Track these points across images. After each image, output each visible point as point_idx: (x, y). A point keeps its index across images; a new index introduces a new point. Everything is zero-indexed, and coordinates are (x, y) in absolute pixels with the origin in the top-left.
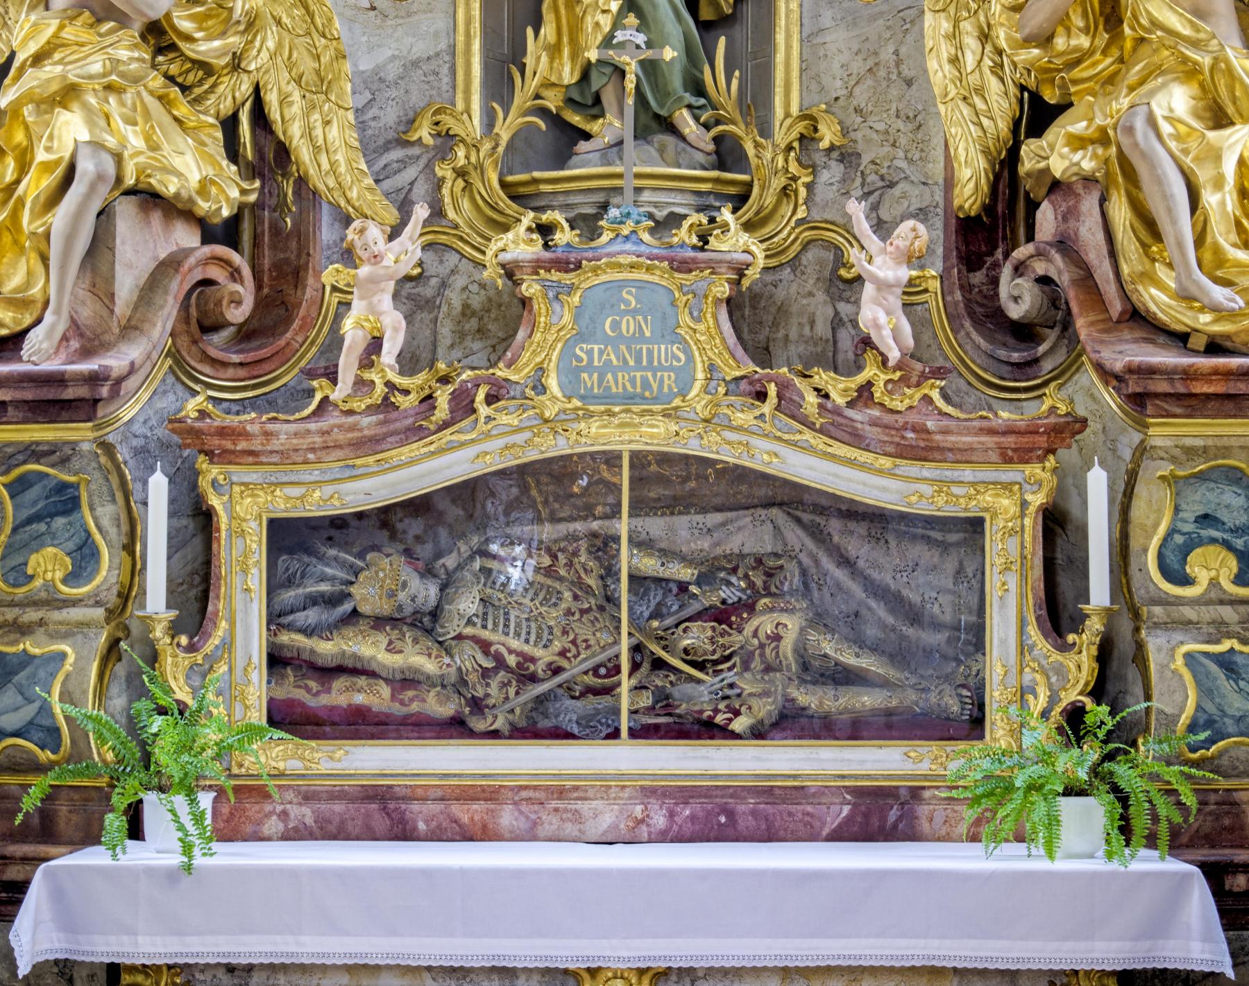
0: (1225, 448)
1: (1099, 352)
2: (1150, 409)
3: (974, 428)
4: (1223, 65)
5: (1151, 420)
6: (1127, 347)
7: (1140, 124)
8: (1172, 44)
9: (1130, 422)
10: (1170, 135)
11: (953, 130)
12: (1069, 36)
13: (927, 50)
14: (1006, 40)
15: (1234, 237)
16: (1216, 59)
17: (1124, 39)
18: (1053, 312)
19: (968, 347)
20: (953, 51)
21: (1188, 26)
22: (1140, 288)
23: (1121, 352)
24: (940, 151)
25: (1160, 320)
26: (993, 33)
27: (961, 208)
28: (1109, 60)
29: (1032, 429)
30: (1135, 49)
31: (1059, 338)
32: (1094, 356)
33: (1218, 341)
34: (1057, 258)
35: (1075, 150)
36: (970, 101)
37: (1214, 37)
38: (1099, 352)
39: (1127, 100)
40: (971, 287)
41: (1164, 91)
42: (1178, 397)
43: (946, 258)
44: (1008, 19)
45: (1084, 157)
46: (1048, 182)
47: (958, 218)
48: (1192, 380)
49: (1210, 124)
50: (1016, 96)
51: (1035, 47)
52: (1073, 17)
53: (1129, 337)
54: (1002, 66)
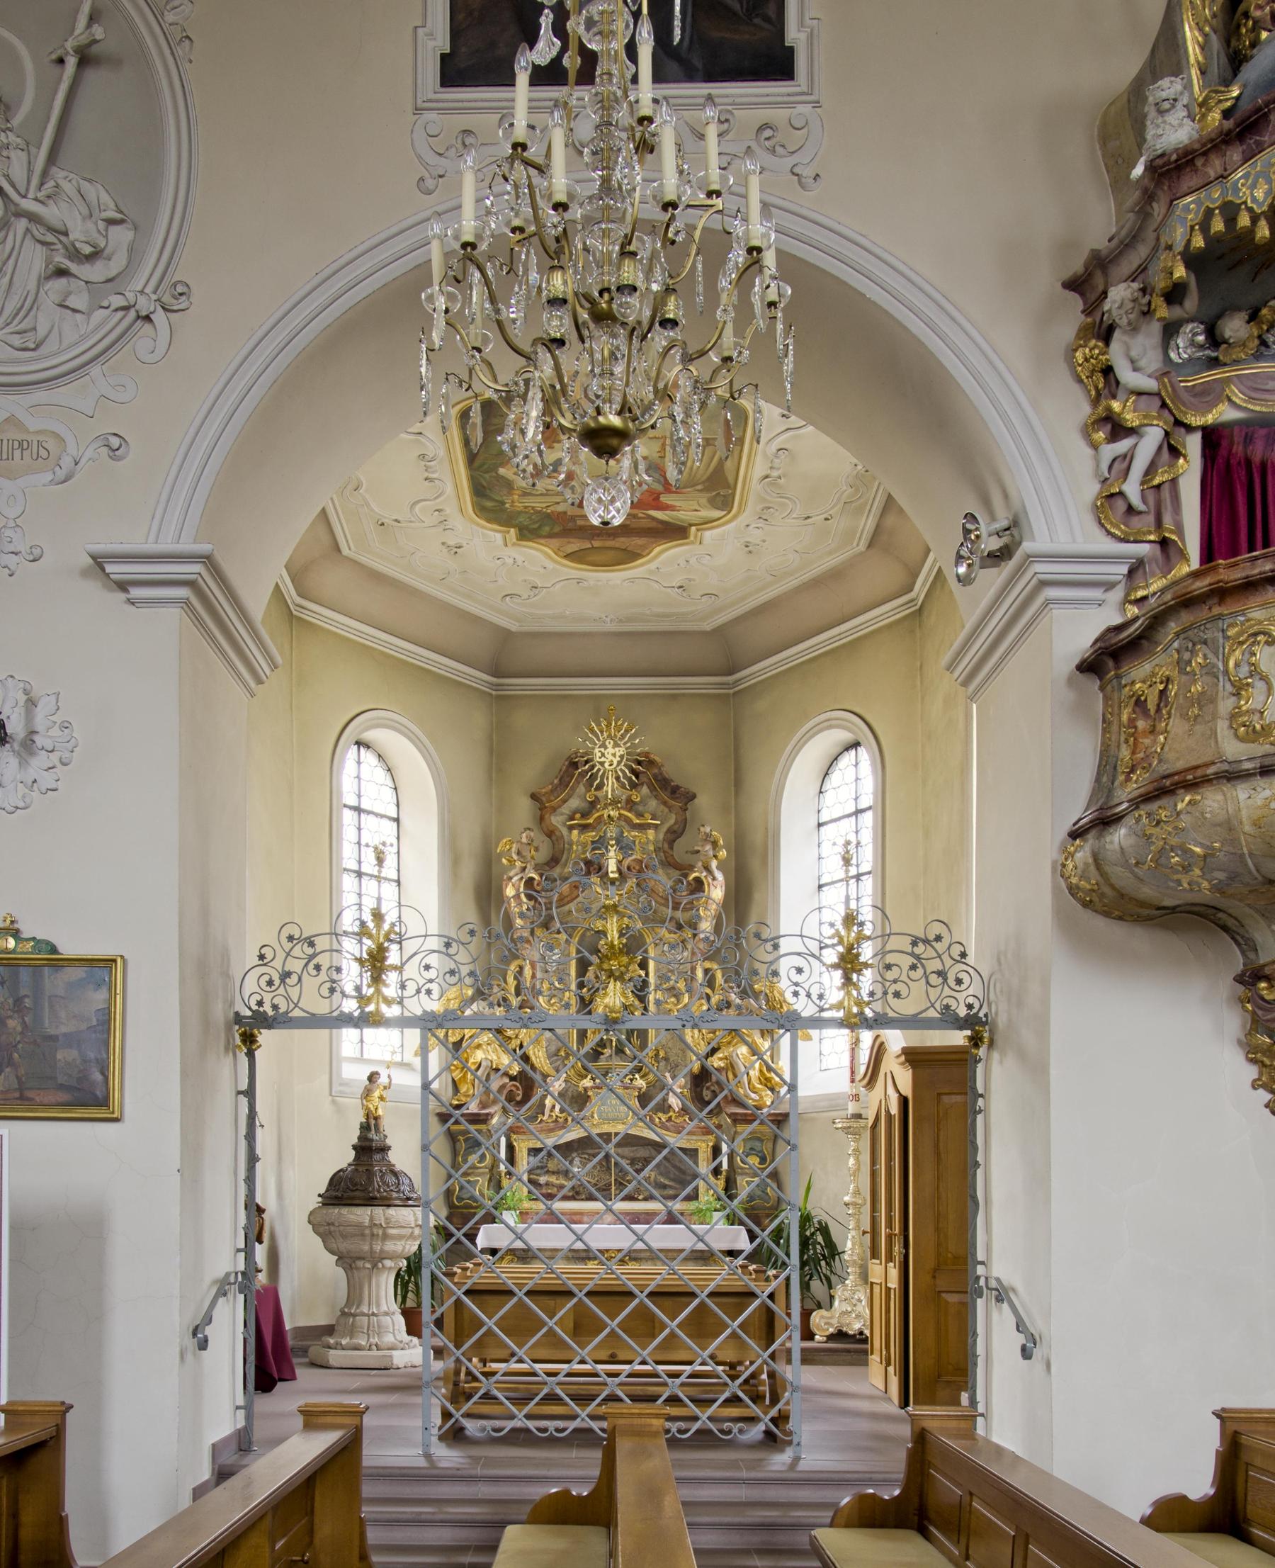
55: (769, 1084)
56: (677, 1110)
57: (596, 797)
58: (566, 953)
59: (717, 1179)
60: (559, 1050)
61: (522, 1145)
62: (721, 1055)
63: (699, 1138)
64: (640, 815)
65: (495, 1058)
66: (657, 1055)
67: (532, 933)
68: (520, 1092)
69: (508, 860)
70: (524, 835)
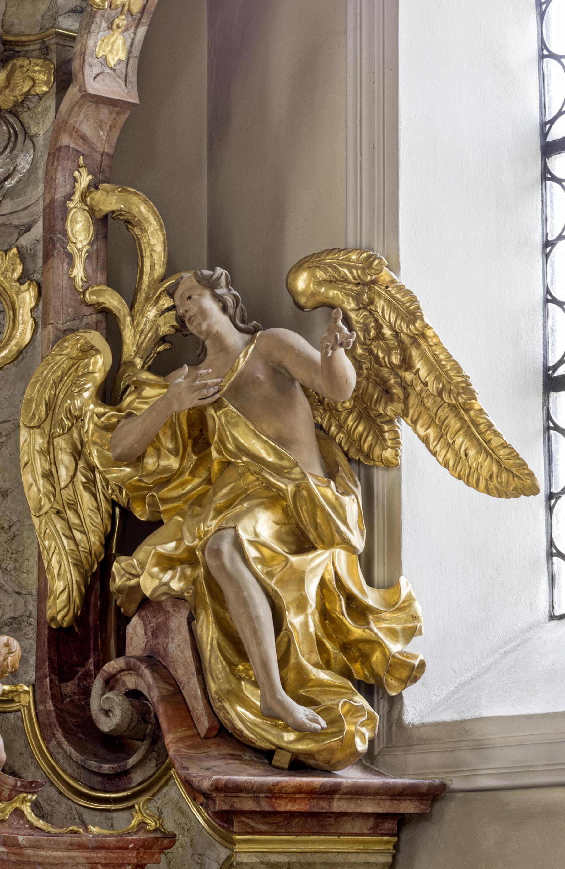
0: (309, 864)
1: (187, 769)
2: (236, 827)
3: (65, 842)
4: (305, 493)
5: (238, 837)
6: (215, 763)
7: (226, 547)
8: (257, 469)
9: (217, 838)
10: (255, 558)
11: (47, 543)
12: (159, 457)
13: (22, 464)
14: (99, 458)
15: (316, 657)
16: (298, 486)
17: (212, 461)
18: (143, 726)
19: (59, 757)
20: (47, 467)
21: (272, 453)
22: (227, 705)
23: (208, 769)
24: (34, 562)
25: (246, 737)
26: (86, 450)
27: (54, 619)
28: (197, 481)
29: (122, 844)
30: (221, 472)
31: (148, 751)
32: (183, 772)
33: (302, 758)
34: (147, 673)
35: (164, 570)
36: (63, 515)
37: (296, 465)
38: (187, 769)
39: (214, 522)
40: (63, 696)
41: (250, 515)
42: (263, 815)
43: (38, 668)
44: (100, 437)
45: (173, 578)
46: (139, 599)
47: (50, 628)
48: (276, 798)
49: (293, 547)
50: (107, 511)
51: (126, 466)
52: (163, 439)
53: (216, 753)
54: (94, 482)
55: (357, 668)
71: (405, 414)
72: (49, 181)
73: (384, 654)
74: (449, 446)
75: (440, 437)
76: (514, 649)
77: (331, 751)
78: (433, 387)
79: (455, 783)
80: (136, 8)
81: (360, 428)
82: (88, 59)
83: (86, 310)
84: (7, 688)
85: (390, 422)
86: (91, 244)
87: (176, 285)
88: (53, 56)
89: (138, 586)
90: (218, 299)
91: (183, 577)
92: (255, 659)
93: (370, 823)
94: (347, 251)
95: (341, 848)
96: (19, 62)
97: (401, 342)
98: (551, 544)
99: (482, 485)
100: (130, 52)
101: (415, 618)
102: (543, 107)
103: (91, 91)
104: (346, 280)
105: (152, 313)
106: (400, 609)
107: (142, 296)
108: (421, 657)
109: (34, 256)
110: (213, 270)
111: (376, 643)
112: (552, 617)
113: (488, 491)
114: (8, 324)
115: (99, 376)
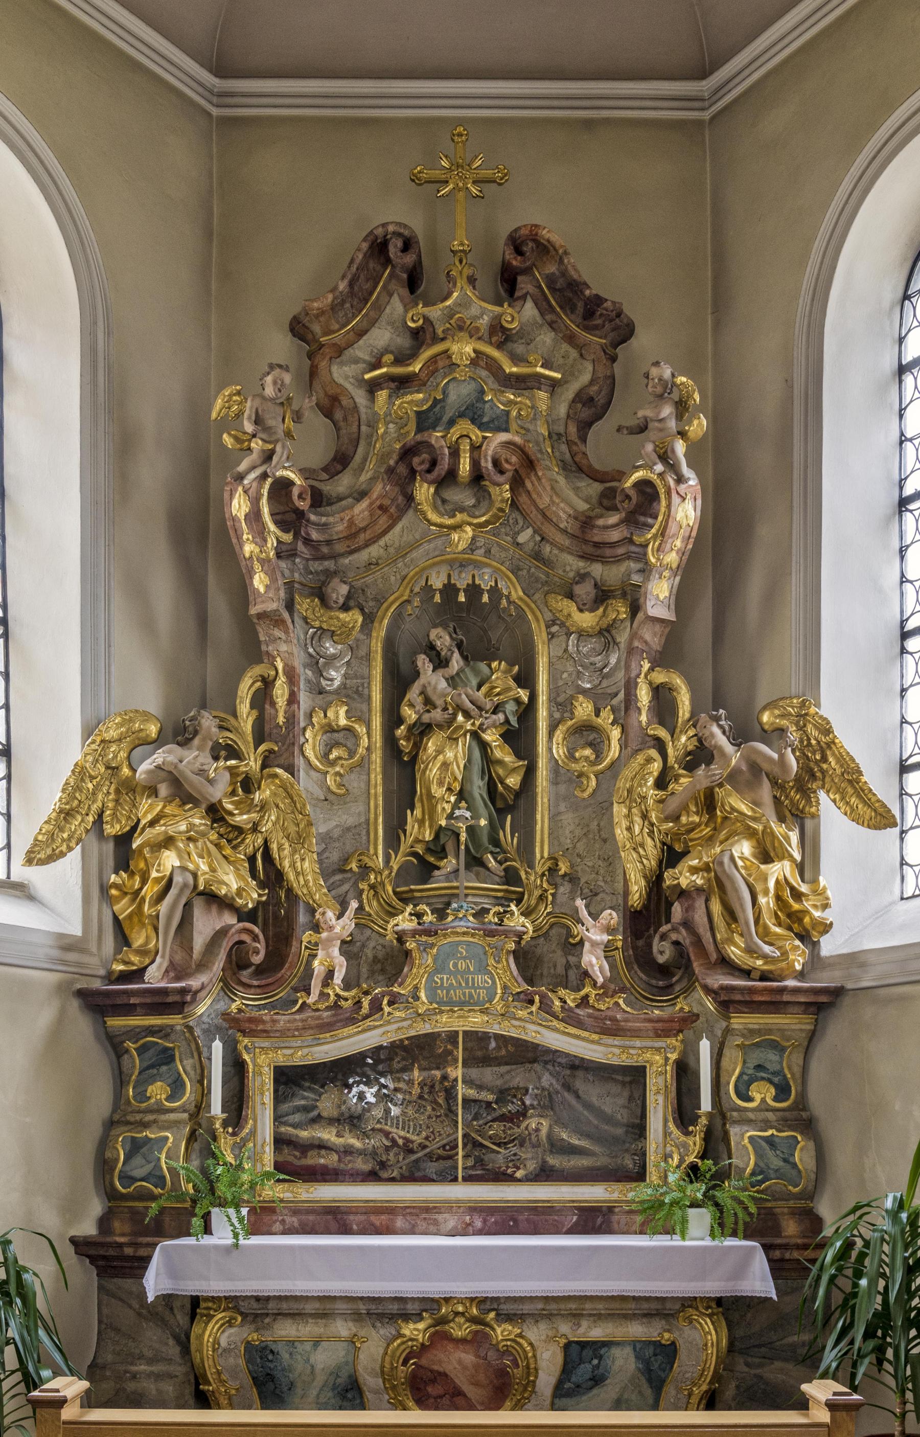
7: (726, 860)
12: (688, 816)
15: (774, 920)
16: (765, 827)
24: (621, 878)
27: (632, 906)
28: (709, 829)
30: (722, 823)
31: (684, 973)
33: (766, 974)
34: (683, 931)
35: (693, 874)
55: (796, 926)
56: (600, 980)
57: (426, 319)
58: (362, 652)
59: (687, 1133)
60: (346, 860)
61: (262, 1059)
62: (695, 862)
63: (648, 1043)
64: (516, 359)
65: (204, 867)
66: (553, 870)
67: (290, 606)
68: (261, 946)
69: (236, 439)
70: (269, 379)
71: (823, 787)
72: (628, 668)
73: (811, 918)
74: (847, 803)
75: (843, 799)
76: (881, 916)
77: (782, 969)
78: (838, 771)
79: (849, 986)
80: (674, 566)
81: (798, 797)
82: (649, 596)
83: (648, 739)
84: (610, 938)
85: (815, 792)
86: (650, 702)
87: (698, 721)
88: (629, 597)
89: (679, 884)
90: (721, 727)
91: (703, 877)
92: (741, 920)
93: (803, 1008)
94: (791, 698)
95: (787, 1021)
96: (610, 602)
97: (821, 747)
98: (902, 858)
99: (866, 824)
100: (671, 592)
101: (827, 899)
102: (902, 612)
103: (650, 614)
104: (790, 714)
105: (683, 739)
106: (819, 894)
107: (678, 730)
108: (831, 919)
109: (619, 710)
110: (718, 711)
111: (806, 912)
112: (902, 899)
113: (869, 827)
114: (606, 748)
115: (656, 774)
